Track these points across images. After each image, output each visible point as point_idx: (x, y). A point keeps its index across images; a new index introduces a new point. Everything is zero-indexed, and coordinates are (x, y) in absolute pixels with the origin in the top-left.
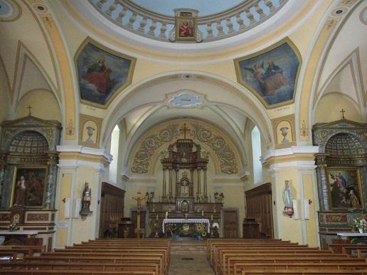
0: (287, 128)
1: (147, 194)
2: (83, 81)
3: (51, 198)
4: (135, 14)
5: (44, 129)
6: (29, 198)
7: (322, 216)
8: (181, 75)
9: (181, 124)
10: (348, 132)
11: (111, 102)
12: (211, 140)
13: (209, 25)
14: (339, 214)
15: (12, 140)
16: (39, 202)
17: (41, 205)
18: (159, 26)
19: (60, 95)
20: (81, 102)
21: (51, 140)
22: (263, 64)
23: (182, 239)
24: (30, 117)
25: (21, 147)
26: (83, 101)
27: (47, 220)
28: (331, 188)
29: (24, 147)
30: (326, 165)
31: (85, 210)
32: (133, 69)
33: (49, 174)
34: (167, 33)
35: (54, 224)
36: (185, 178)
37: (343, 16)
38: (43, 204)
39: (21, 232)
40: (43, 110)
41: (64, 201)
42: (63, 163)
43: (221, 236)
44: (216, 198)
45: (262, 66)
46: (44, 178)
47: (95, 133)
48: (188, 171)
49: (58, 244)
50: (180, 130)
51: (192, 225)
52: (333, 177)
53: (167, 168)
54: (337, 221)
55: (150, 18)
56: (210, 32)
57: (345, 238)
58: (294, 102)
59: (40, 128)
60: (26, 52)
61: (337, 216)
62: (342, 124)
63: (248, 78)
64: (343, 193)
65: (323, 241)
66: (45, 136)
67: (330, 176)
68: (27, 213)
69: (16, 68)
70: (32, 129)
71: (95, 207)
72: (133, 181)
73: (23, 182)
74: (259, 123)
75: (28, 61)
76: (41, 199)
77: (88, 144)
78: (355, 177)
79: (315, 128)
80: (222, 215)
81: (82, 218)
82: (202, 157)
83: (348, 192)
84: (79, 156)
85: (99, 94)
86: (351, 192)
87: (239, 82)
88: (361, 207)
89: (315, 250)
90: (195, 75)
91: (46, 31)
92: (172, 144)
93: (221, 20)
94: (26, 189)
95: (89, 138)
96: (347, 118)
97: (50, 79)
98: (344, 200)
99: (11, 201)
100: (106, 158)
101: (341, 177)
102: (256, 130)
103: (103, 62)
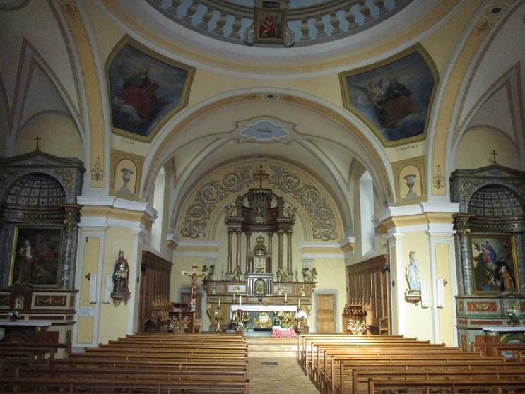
0: (415, 176)
1: (205, 268)
2: (116, 100)
3: (69, 273)
4: (239, 19)
5: (59, 170)
6: (37, 272)
7: (462, 303)
8: (260, 94)
9: (254, 166)
10: (500, 183)
11: (156, 133)
12: (299, 190)
13: (305, 22)
14: (486, 300)
15: (12, 187)
16: (53, 277)
17: (54, 283)
18: (230, 20)
19: (82, 122)
20: (113, 132)
21: (70, 187)
22: (381, 81)
23: (257, 334)
24: (37, 153)
25: (24, 196)
26: (117, 130)
27: (65, 305)
28: (475, 263)
29: (29, 197)
30: (469, 230)
31: (120, 292)
32: (190, 85)
33: (66, 237)
34: (241, 32)
35: (74, 312)
36: (260, 247)
37: (502, 16)
38: (58, 282)
39: (26, 322)
40: (59, 143)
41: (88, 277)
42: (85, 221)
43: (312, 330)
44: (305, 275)
45: (380, 84)
46: (58, 242)
47: (133, 178)
48: (265, 235)
49: (78, 345)
50: (254, 175)
51: (272, 314)
52: (478, 248)
53: (235, 231)
54: (483, 310)
55: (217, 9)
56: (305, 32)
57: (494, 334)
58: (425, 138)
59: (53, 170)
60: (35, 56)
61: (483, 303)
62: (492, 171)
63: (359, 102)
64: (491, 270)
65: (462, 339)
66: (61, 182)
67: (473, 246)
68: (35, 294)
69: (18, 80)
70: (41, 171)
71: (133, 286)
72: (183, 249)
73: (29, 248)
74: (371, 166)
75: (36, 70)
76: (55, 273)
77: (124, 194)
78: (509, 247)
79: (454, 177)
80: (313, 300)
81: (114, 301)
82: (286, 215)
83: (498, 269)
84: (110, 211)
85: (138, 119)
86: (503, 269)
87: (345, 106)
88: (516, 290)
89: (452, 352)
90: (280, 95)
91: (65, 26)
92: (242, 195)
93: (322, 15)
94: (33, 259)
95: (124, 186)
96: (500, 163)
97: (68, 96)
98: (492, 280)
99: (10, 278)
100: (150, 216)
101: (489, 248)
102: (367, 176)
103: (147, 73)
